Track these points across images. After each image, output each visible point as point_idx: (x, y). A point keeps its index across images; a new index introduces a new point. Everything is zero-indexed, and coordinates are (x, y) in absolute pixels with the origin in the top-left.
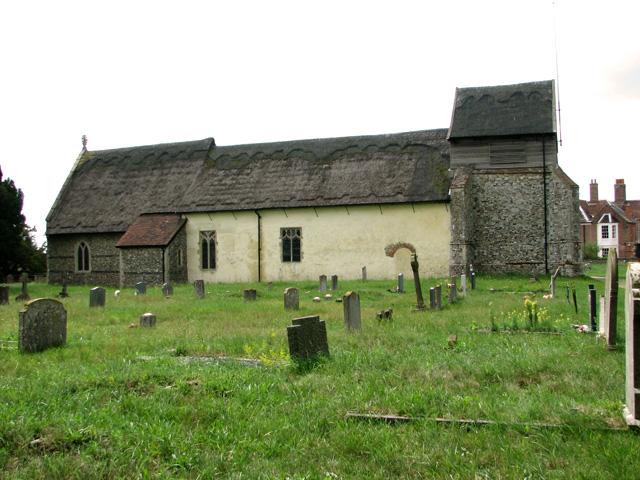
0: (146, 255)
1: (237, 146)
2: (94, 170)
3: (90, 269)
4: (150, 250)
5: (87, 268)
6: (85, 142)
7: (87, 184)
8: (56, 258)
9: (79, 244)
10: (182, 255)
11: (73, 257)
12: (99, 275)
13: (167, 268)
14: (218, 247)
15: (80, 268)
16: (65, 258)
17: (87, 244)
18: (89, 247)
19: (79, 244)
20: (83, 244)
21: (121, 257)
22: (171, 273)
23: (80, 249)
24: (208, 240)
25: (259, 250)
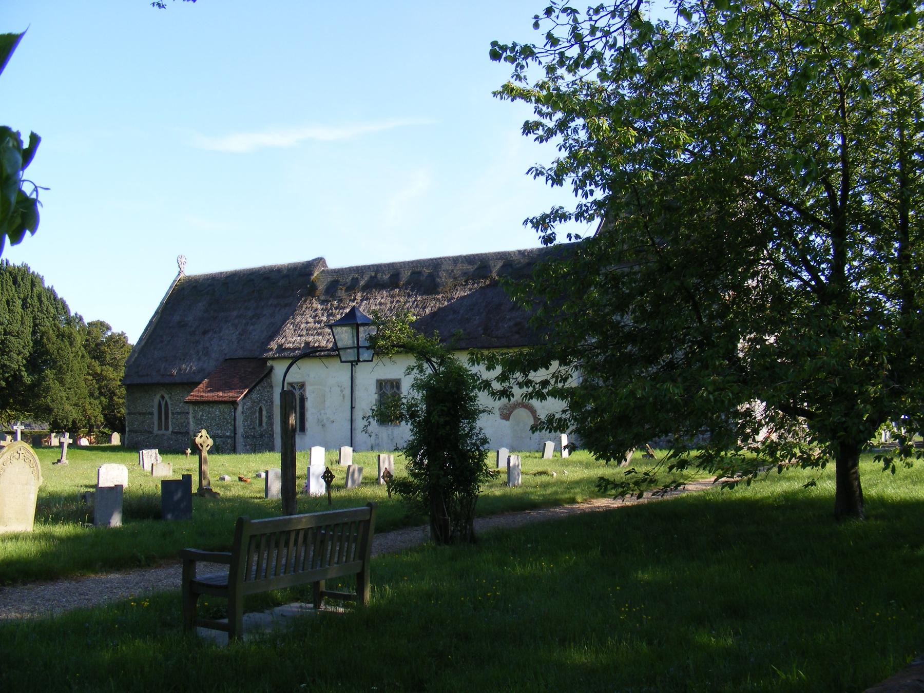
0: (217, 413)
1: (365, 266)
2: (593, 219)
3: (171, 429)
4: (222, 407)
5: (167, 429)
6: (539, 173)
7: (177, 318)
8: (135, 414)
9: (158, 397)
10: (264, 413)
11: (152, 414)
12: (179, 436)
13: (240, 430)
14: (309, 404)
15: (160, 428)
16: (144, 414)
17: (167, 397)
18: (169, 402)
19: (158, 397)
20: (163, 397)
21: (191, 416)
22: (246, 437)
23: (160, 405)
24: (389, 392)
25: (352, 408)
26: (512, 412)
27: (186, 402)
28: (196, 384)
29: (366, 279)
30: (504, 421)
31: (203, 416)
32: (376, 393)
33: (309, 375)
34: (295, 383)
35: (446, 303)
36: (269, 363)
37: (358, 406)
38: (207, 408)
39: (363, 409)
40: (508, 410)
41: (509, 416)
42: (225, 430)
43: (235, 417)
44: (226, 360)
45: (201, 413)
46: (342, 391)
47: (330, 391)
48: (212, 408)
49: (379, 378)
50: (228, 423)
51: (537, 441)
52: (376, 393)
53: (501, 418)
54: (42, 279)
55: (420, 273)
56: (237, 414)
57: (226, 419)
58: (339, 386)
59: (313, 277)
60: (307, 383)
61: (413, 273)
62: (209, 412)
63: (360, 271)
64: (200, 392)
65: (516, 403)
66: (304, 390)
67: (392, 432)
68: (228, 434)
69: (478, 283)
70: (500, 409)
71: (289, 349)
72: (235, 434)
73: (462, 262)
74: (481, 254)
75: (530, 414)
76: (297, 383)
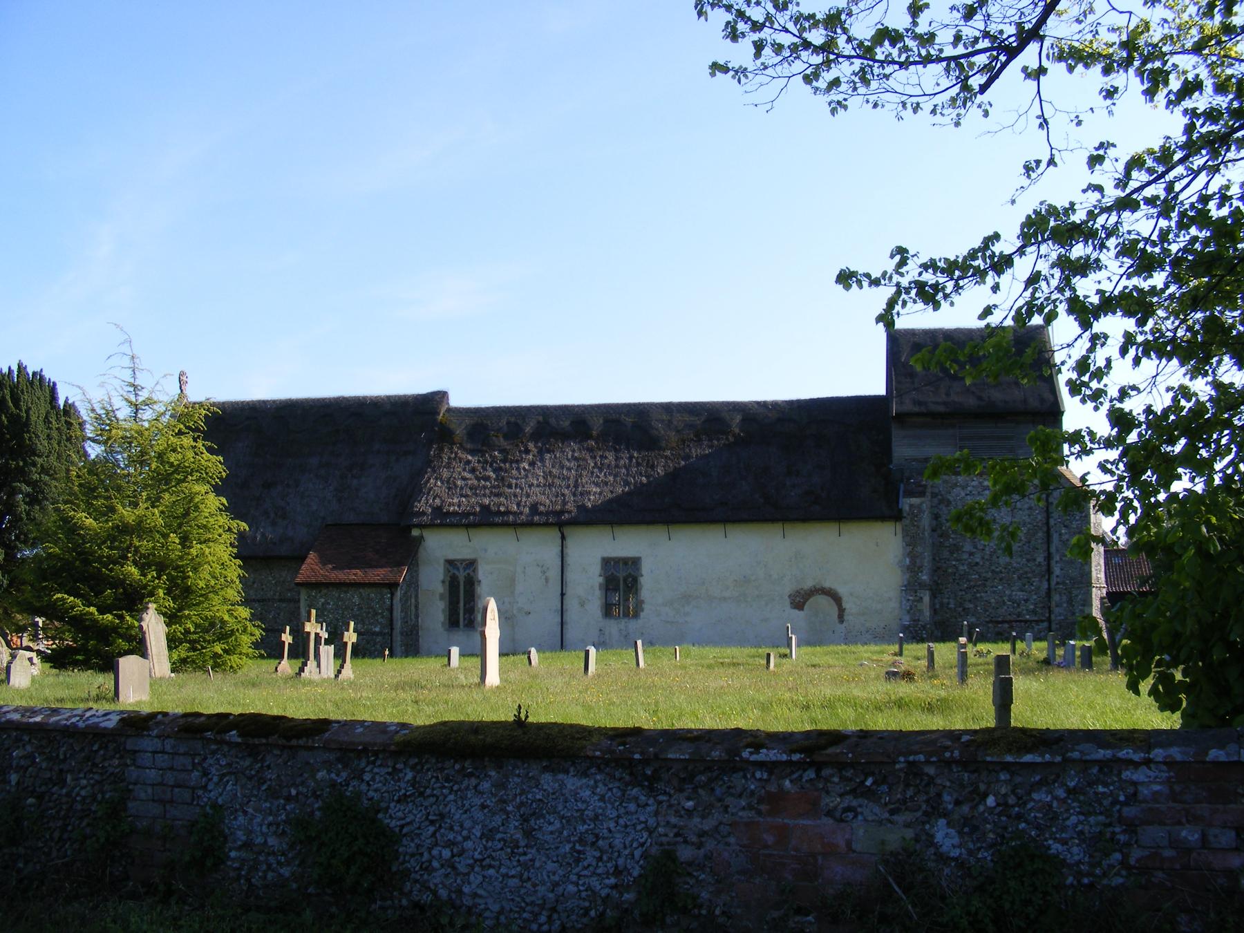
0: (356, 600)
4: (364, 592)
25: (562, 595)
26: (807, 600)
27: (298, 584)
28: (303, 559)
29: (532, 424)
30: (796, 611)
31: (329, 604)
32: (600, 576)
33: (486, 550)
34: (458, 560)
35: (683, 463)
36: (415, 532)
37: (570, 591)
38: (335, 593)
39: (579, 597)
40: (803, 598)
41: (804, 603)
42: (371, 624)
43: (392, 605)
44: (327, 525)
45: (323, 600)
46: (544, 572)
47: (524, 572)
48: (346, 592)
49: (606, 555)
50: (376, 614)
51: (843, 634)
52: (600, 576)
53: (791, 608)
54: (1063, 412)
55: (618, 422)
56: (394, 602)
57: (372, 608)
58: (538, 565)
59: (440, 417)
60: (479, 561)
61: (606, 421)
62: (339, 598)
63: (545, 413)
64: (312, 567)
65: (813, 589)
66: (474, 571)
67: (626, 627)
68: (377, 629)
69: (718, 440)
70: (790, 596)
71: (455, 514)
72: (392, 629)
73: (679, 411)
74: (714, 402)
75: (832, 602)
76: (462, 561)
